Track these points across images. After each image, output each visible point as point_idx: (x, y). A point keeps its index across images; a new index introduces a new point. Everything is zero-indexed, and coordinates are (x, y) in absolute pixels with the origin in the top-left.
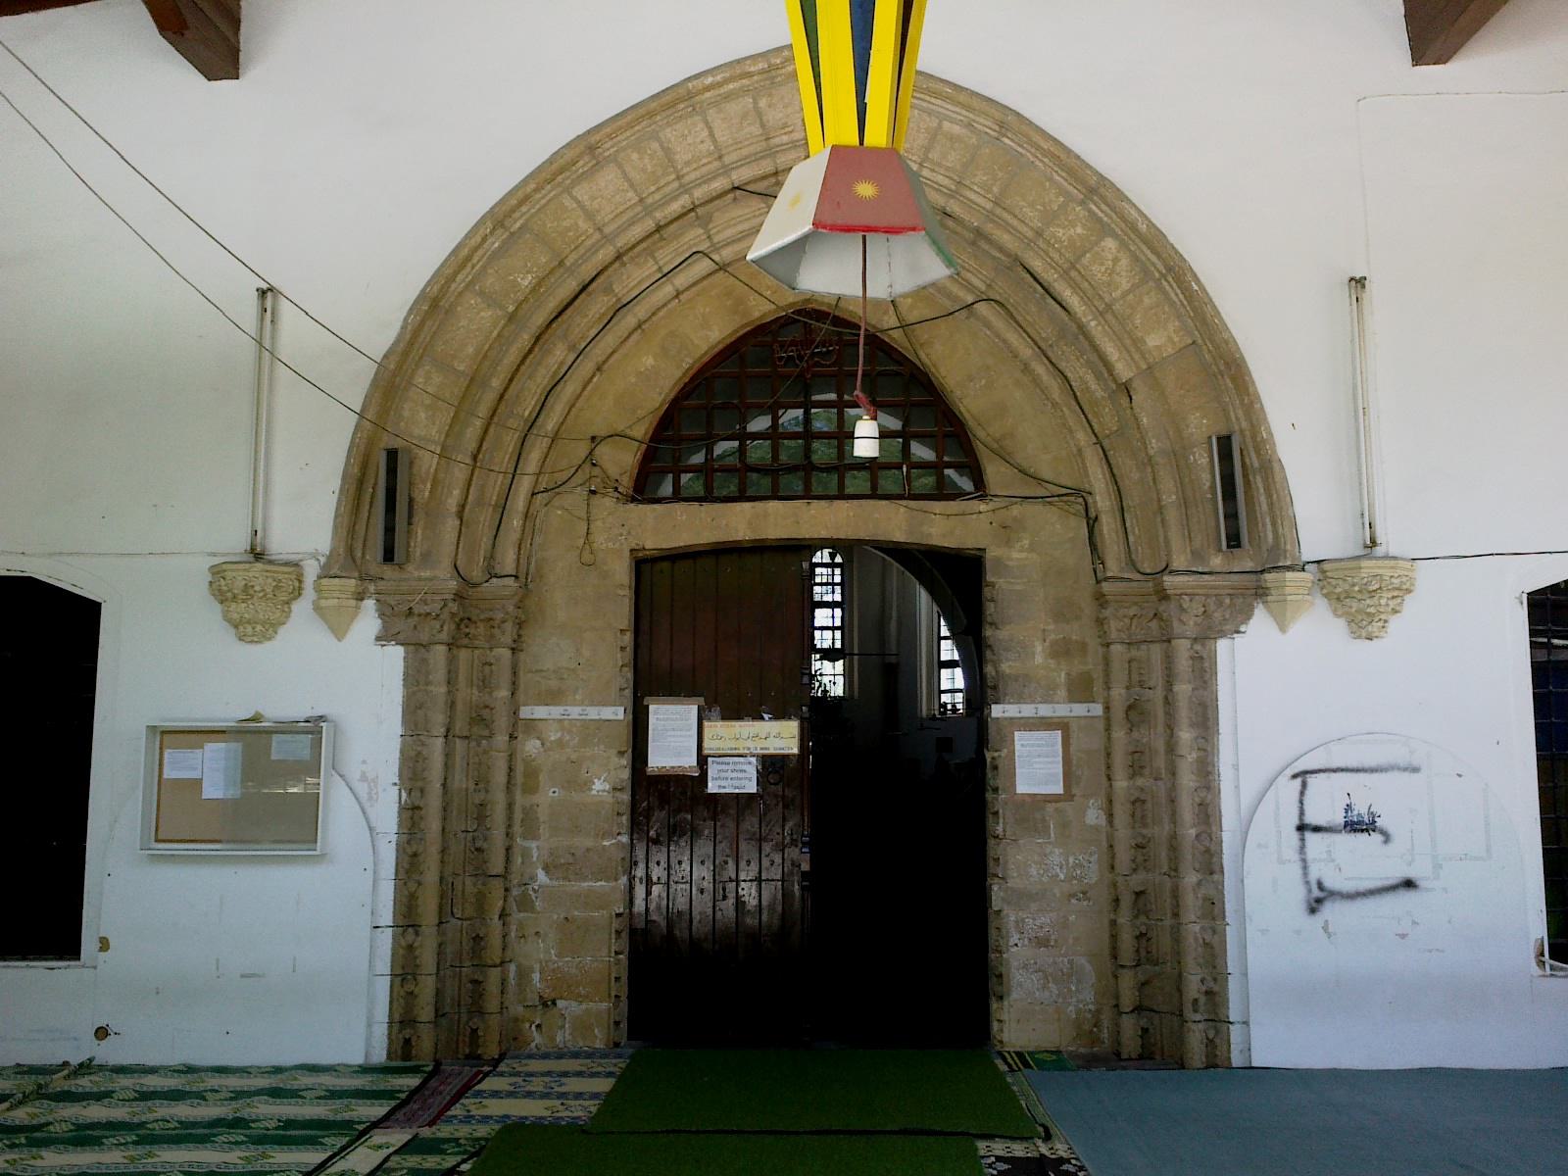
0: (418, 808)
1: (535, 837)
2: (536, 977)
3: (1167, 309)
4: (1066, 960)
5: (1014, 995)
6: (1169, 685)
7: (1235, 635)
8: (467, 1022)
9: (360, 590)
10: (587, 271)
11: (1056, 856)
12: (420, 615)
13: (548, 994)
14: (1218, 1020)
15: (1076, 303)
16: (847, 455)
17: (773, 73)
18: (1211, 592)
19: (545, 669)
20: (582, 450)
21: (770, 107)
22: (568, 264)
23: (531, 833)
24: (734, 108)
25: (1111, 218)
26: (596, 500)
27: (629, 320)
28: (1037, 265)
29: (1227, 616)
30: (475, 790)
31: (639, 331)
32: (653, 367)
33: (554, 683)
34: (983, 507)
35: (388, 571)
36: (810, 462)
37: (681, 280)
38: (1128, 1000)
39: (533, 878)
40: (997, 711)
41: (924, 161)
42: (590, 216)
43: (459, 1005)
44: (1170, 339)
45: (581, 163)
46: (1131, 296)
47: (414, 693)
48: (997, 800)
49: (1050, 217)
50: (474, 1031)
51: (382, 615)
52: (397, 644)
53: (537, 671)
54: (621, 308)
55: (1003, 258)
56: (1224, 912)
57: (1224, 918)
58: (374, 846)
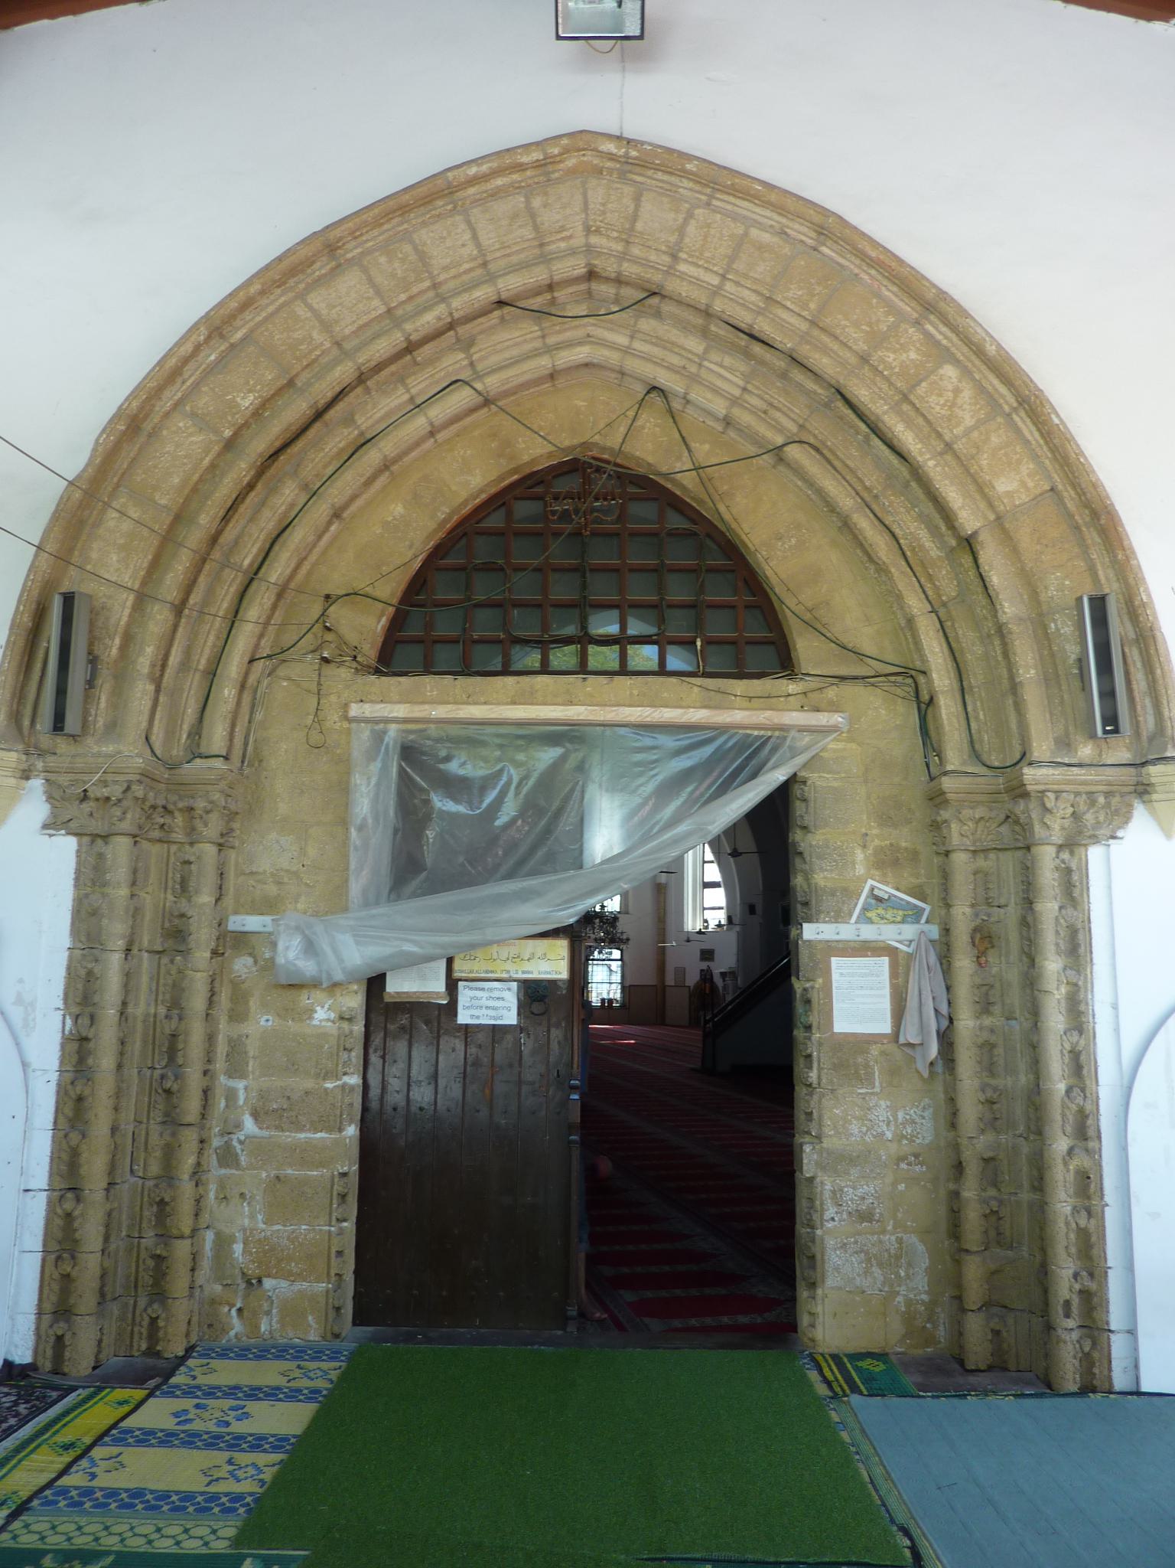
0: (86, 1039)
1: (243, 1076)
2: (238, 1248)
3: (1018, 449)
4: (893, 1238)
5: (830, 1282)
6: (1028, 902)
7: (1111, 841)
8: (145, 1310)
9: (24, 766)
10: (323, 390)
11: (881, 1110)
12: (97, 800)
13: (253, 1270)
14: (1094, 1329)
15: (910, 440)
16: (632, 610)
17: (550, 168)
18: (1081, 788)
19: (261, 870)
20: (316, 610)
21: (545, 206)
22: (299, 384)
23: (236, 1070)
24: (502, 208)
25: (951, 341)
26: (328, 670)
27: (372, 457)
28: (862, 394)
29: (1101, 819)
30: (167, 1017)
31: (387, 474)
32: (402, 516)
33: (272, 889)
34: (792, 687)
35: (62, 745)
36: (586, 634)
37: (438, 412)
38: (975, 1293)
39: (239, 1126)
40: (810, 931)
41: (727, 271)
42: (326, 326)
43: (136, 1287)
44: (1023, 484)
45: (318, 265)
46: (975, 434)
47: (87, 896)
48: (809, 1039)
49: (878, 340)
50: (154, 1321)
51: (50, 798)
52: (68, 834)
53: (252, 873)
54: (363, 444)
55: (820, 391)
56: (1102, 1189)
57: (1102, 1197)
58: (27, 1086)
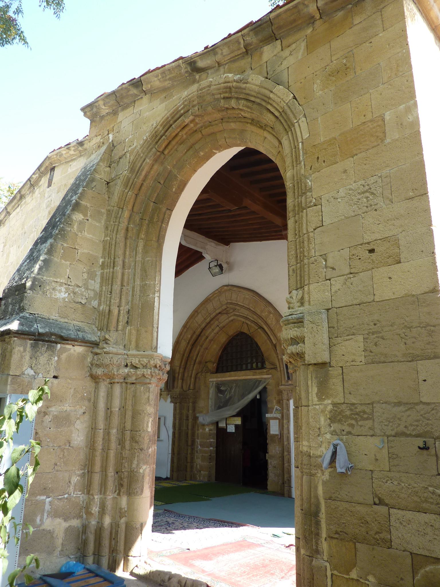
34: (265, 371)
42: (197, 323)
54: (207, 337)
